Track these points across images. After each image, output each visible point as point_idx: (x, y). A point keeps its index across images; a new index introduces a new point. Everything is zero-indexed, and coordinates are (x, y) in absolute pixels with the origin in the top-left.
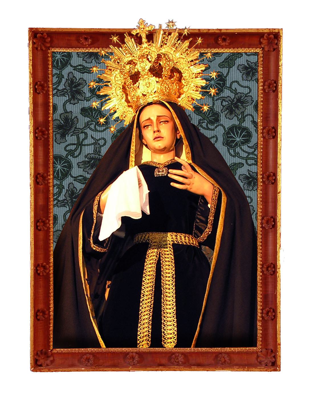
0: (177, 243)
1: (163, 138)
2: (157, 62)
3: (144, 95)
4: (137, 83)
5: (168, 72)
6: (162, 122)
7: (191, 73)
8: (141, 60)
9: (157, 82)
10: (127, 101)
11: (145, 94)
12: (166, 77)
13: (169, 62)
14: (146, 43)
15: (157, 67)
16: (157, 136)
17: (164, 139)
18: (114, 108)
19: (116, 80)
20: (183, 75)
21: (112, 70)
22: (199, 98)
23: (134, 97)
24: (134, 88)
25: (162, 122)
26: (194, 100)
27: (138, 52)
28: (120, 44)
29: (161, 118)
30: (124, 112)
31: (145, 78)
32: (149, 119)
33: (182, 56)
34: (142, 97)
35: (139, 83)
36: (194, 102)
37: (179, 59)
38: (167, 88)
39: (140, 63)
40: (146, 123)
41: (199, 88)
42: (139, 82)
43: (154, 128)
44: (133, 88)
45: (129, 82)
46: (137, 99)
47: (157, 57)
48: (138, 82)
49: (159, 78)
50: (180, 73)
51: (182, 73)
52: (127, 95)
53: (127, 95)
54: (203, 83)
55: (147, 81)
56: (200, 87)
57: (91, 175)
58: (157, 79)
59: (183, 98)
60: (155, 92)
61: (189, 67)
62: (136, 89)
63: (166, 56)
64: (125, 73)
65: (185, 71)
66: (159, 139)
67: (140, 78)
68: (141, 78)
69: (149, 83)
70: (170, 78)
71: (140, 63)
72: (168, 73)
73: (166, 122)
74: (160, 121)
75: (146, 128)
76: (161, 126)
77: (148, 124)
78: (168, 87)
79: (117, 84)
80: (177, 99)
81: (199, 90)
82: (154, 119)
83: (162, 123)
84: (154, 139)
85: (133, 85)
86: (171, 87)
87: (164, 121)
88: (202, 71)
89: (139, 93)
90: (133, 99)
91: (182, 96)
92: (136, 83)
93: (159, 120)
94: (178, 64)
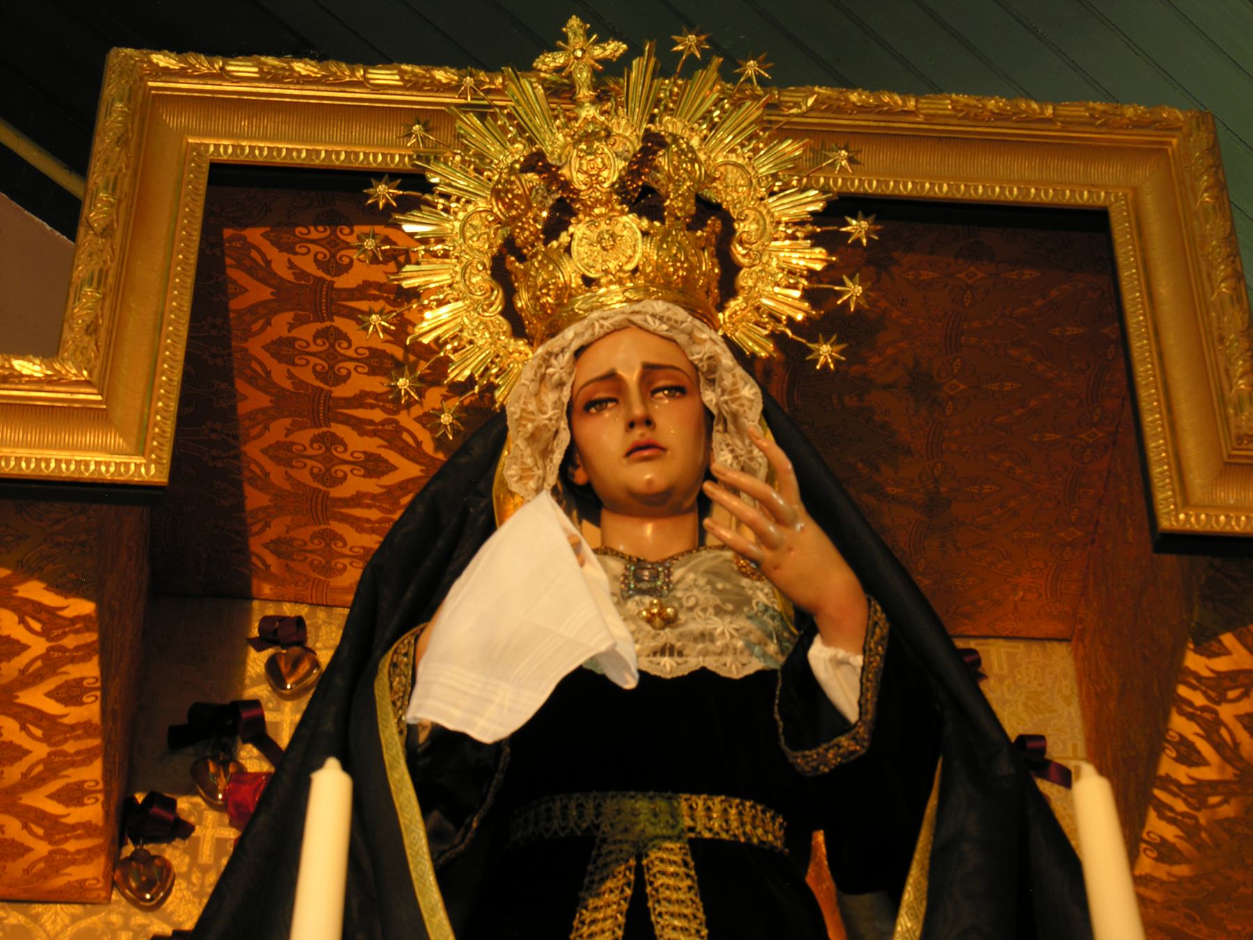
0: (835, 741)
1: (664, 449)
2: (638, 169)
3: (588, 282)
4: (564, 238)
5: (686, 201)
6: (661, 389)
7: (768, 220)
8: (583, 146)
9: (645, 234)
10: (509, 312)
11: (592, 274)
12: (678, 218)
13: (693, 166)
14: (593, 103)
15: (635, 190)
16: (643, 440)
17: (669, 453)
18: (454, 337)
19: (468, 234)
20: (740, 227)
21: (454, 198)
22: (800, 317)
23: (544, 291)
24: (550, 255)
25: (661, 389)
26: (778, 321)
27: (560, 136)
28: (418, 198)
29: (660, 373)
30: (497, 356)
31: (599, 216)
32: (612, 376)
33: (733, 158)
34: (579, 287)
35: (572, 236)
36: (781, 328)
37: (722, 169)
38: (682, 263)
39: (581, 158)
40: (596, 392)
41: (801, 276)
42: (571, 229)
43: (629, 408)
44: (545, 255)
45: (527, 233)
46: (557, 297)
47: (640, 151)
48: (566, 229)
49: (651, 219)
50: (728, 222)
51: (734, 220)
52: (510, 294)
53: (510, 294)
54: (814, 258)
55: (604, 227)
56: (805, 272)
57: (347, 611)
58: (645, 223)
59: (735, 312)
60: (636, 270)
61: (762, 199)
62: (555, 257)
63: (681, 141)
64: (516, 196)
65: (747, 212)
66: (646, 453)
67: (575, 214)
68: (581, 216)
69: (613, 236)
70: (691, 227)
71: (581, 158)
72: (688, 207)
73: (678, 394)
74: (651, 389)
75: (593, 410)
76: (657, 407)
77: (602, 395)
78: (686, 258)
79: (471, 248)
80: (713, 310)
81: (801, 286)
82: (631, 377)
83: (660, 394)
84: (628, 454)
85: (546, 244)
86: (694, 260)
87: (670, 388)
88: (813, 213)
89: (569, 273)
90: (543, 300)
91: (733, 304)
92: (556, 237)
93: (651, 383)
94: (720, 187)
